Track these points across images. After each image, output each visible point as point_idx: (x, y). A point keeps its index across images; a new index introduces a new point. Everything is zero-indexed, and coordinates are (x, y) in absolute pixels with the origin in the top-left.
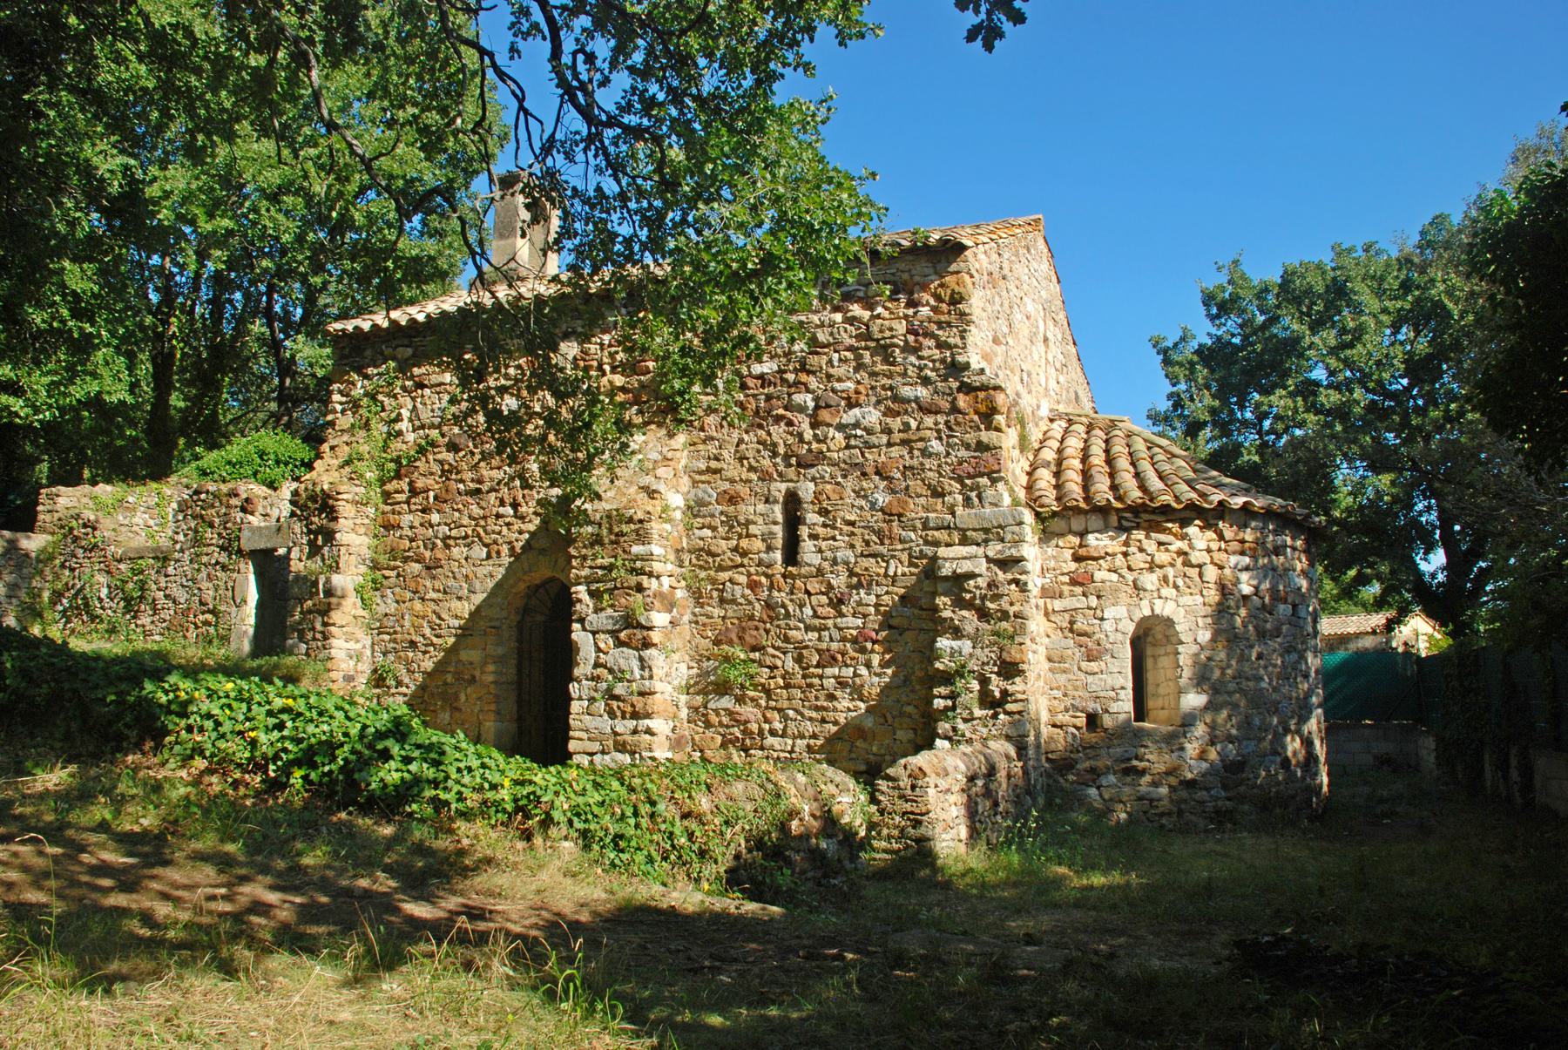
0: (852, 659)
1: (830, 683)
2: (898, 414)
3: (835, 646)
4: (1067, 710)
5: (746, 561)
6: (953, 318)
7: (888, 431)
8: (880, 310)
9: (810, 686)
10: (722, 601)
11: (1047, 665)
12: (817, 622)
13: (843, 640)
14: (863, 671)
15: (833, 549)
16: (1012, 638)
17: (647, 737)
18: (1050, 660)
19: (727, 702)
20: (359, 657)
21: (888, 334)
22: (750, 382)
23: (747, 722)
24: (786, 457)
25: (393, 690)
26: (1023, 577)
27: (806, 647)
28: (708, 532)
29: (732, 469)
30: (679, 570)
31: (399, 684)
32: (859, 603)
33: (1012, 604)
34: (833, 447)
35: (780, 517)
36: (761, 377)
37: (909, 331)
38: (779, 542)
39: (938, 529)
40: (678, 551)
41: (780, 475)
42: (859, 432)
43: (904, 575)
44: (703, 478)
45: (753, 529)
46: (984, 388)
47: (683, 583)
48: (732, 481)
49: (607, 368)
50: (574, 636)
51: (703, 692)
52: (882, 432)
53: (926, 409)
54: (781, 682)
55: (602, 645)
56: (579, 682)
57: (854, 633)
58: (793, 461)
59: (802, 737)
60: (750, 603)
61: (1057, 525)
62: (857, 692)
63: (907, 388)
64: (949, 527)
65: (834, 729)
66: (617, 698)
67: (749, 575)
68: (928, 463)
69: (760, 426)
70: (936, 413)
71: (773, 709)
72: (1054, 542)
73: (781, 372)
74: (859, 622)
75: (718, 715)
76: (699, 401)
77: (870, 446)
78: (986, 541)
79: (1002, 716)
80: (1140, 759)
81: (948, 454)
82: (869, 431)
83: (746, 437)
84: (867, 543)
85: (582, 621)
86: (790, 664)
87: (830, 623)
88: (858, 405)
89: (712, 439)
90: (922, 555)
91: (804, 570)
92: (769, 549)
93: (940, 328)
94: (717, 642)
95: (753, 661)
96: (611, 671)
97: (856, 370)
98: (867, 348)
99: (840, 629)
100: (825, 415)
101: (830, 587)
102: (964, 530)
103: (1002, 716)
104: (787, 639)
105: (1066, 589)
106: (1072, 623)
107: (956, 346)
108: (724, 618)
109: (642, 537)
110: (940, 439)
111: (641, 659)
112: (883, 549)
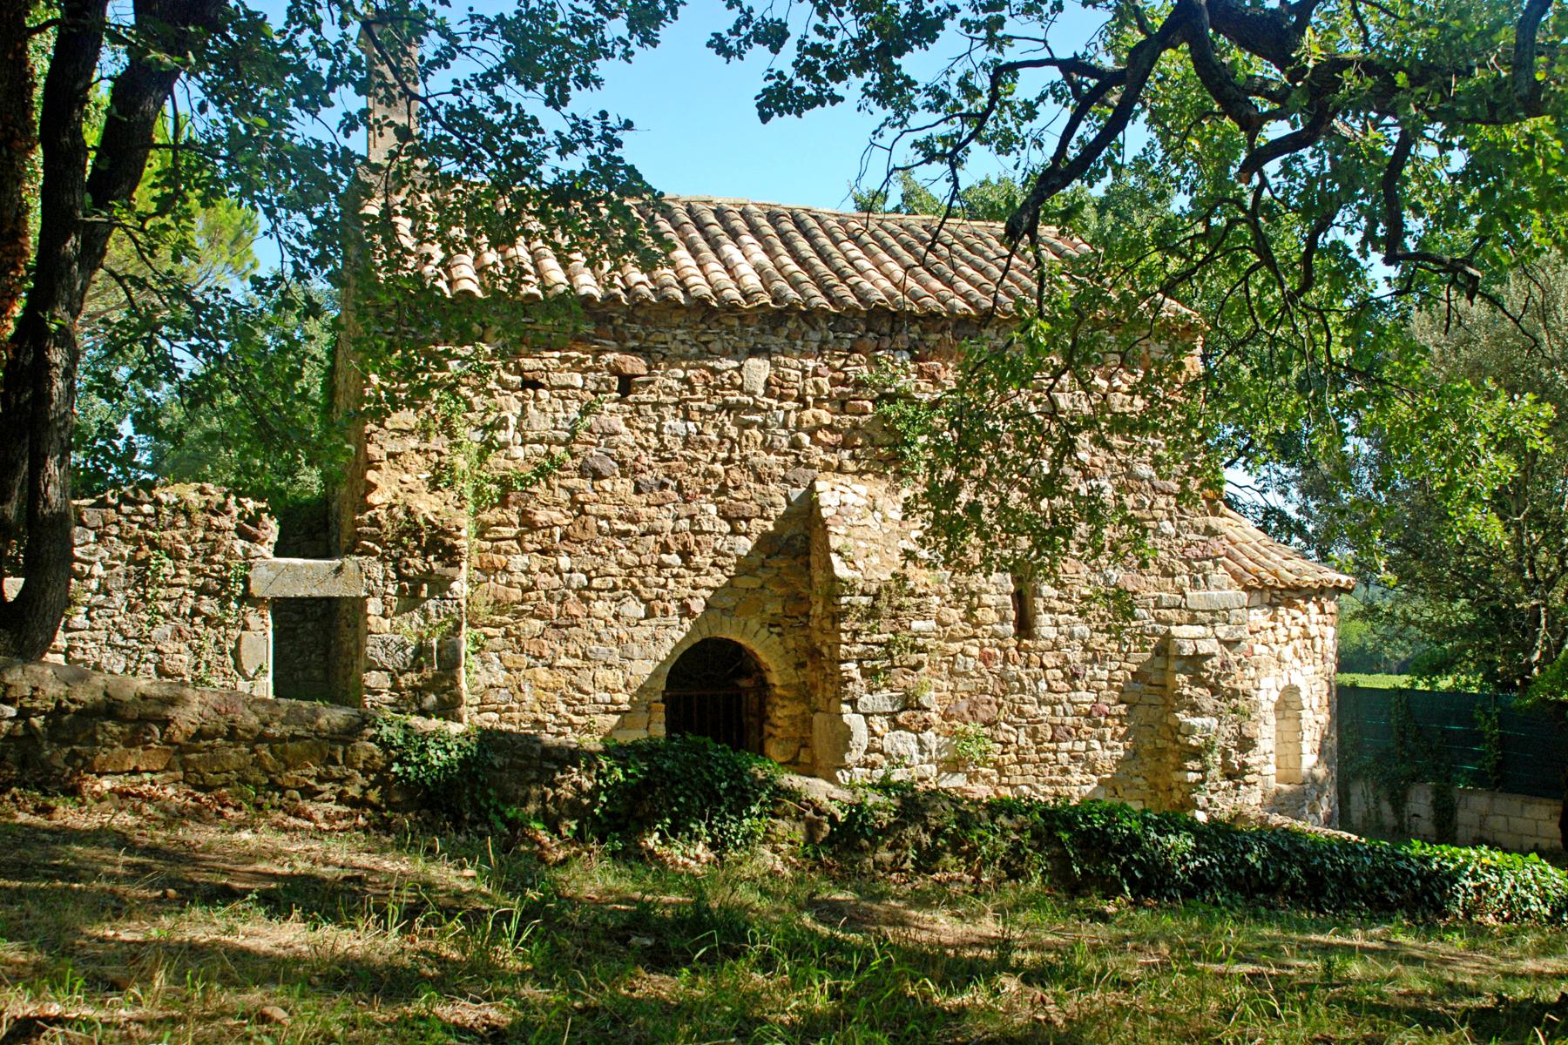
81: (1178, 536)
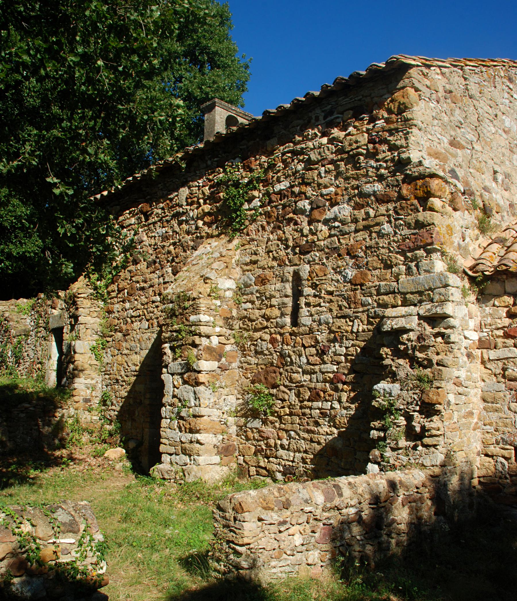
0: (330, 395)
1: (316, 413)
2: (362, 207)
3: (319, 385)
4: (498, 443)
6: (399, 125)
7: (355, 221)
8: (351, 129)
9: (304, 414)
10: (257, 352)
11: (482, 405)
12: (309, 367)
13: (325, 381)
14: (336, 405)
15: (319, 313)
16: (430, 382)
17: (198, 445)
18: (484, 400)
19: (257, 424)
20: (94, 388)
21: (355, 146)
22: (274, 197)
23: (268, 438)
24: (294, 248)
25: (110, 408)
26: (448, 331)
27: (302, 386)
28: (249, 305)
29: (264, 260)
30: (229, 332)
31: (112, 404)
32: (335, 354)
33: (438, 354)
34: (320, 237)
35: (289, 292)
36: (280, 192)
37: (370, 142)
38: (289, 310)
39: (386, 294)
40: (226, 319)
41: (290, 261)
42: (337, 224)
43: (364, 331)
44: (248, 268)
45: (274, 301)
46: (422, 176)
47: (232, 341)
48: (264, 269)
49: (201, 201)
50: (163, 377)
51: (245, 416)
52: (352, 222)
53: (382, 200)
54: (287, 411)
55: (176, 383)
56: (165, 407)
57: (331, 376)
58: (297, 250)
59: (299, 452)
60: (271, 354)
61: (492, 287)
62: (332, 420)
63: (368, 186)
64: (394, 292)
65: (318, 448)
66: (182, 418)
67: (271, 334)
68: (382, 243)
69: (279, 228)
70: (387, 202)
71: (283, 430)
72: (492, 302)
73: (292, 187)
74: (335, 368)
75: (252, 432)
76: (246, 215)
77: (343, 233)
78: (421, 302)
79: (420, 448)
80: (373, 508)
81: (396, 233)
82: (343, 223)
83: (271, 237)
84: (340, 307)
85: (166, 367)
86: (293, 398)
87: (317, 368)
88: (337, 204)
89: (253, 240)
90: (376, 316)
91: (302, 329)
92: (283, 315)
93: (391, 135)
94: (253, 382)
95: (272, 395)
96: (180, 401)
97: (336, 178)
98: (342, 160)
99: (323, 373)
100: (316, 214)
101: (317, 341)
102: (405, 294)
103: (420, 448)
104: (291, 381)
105: (500, 341)
106: (504, 369)
107: (402, 147)
108: (257, 364)
109: (196, 310)
110: (390, 222)
111: (195, 393)
112: (350, 312)
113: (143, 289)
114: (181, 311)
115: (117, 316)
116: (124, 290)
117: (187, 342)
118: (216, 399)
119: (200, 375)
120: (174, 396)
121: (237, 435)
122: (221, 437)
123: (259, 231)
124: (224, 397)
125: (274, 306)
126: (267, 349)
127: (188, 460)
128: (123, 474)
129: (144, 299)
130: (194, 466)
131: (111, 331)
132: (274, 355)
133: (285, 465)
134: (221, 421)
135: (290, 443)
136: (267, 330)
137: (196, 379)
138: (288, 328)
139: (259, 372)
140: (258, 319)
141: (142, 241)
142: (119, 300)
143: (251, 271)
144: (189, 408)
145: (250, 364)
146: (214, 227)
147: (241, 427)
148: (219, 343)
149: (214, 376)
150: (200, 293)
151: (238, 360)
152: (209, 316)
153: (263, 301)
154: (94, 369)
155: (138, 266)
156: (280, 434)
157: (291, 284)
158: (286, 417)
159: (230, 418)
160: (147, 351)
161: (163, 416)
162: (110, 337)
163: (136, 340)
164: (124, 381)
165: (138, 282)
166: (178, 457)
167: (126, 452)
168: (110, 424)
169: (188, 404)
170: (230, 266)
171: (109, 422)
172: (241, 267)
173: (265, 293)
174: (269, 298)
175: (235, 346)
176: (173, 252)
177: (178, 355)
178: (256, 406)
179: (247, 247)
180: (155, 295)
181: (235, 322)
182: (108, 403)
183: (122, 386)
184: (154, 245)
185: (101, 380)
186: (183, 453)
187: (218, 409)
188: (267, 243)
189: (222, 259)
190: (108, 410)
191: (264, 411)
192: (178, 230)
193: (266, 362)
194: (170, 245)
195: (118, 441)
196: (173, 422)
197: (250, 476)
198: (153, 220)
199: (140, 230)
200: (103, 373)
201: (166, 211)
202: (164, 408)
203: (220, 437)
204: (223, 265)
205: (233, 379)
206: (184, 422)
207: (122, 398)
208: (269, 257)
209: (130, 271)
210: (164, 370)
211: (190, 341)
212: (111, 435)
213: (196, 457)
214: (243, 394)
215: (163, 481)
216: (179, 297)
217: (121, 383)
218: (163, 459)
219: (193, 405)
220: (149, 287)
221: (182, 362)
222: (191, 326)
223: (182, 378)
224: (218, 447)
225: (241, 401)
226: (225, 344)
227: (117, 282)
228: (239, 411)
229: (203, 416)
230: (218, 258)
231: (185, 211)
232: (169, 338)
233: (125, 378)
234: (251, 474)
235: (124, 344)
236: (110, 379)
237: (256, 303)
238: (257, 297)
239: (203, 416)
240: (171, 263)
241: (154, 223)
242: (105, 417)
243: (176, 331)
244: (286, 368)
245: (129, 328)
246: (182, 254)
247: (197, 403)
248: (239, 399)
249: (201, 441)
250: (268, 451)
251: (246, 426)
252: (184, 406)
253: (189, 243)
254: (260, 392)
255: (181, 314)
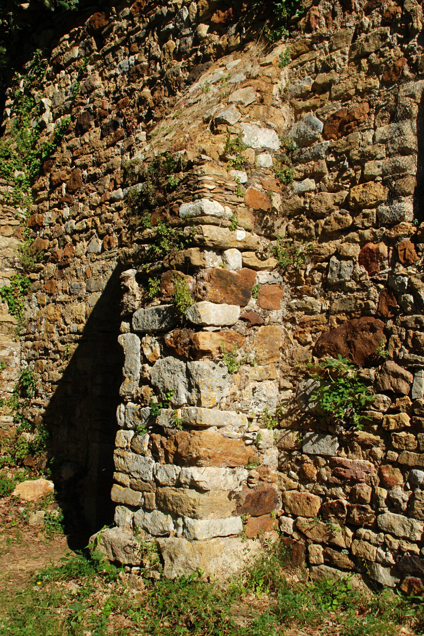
5: (358, 221)
17: (193, 494)
23: (354, 481)
30: (265, 242)
31: (37, 395)
44: (307, 103)
47: (272, 262)
50: (121, 339)
54: (406, 419)
55: (148, 352)
56: (125, 403)
60: (364, 288)
67: (363, 242)
71: (395, 464)
75: (316, 464)
83: (366, 21)
85: (129, 318)
89: (321, 38)
94: (151, 343)
95: (366, 382)
96: (156, 391)
108: (328, 313)
111: (188, 374)
113: (93, 178)
114: (161, 195)
115: (49, 232)
116: (60, 184)
117: (173, 263)
118: (235, 389)
119: (201, 334)
120: (144, 381)
121: (280, 469)
122: (246, 473)
123: (334, 14)
124: (252, 385)
125: (373, 178)
126: (354, 277)
127: (171, 527)
128: (42, 536)
129: (95, 198)
130: (185, 542)
131: (38, 262)
132: (372, 289)
133: (400, 551)
134: (246, 438)
135: (412, 498)
136: (353, 235)
137: (191, 342)
138: (409, 225)
139: (332, 329)
140: (330, 211)
141: (93, 88)
142: (53, 203)
143: (314, 108)
144: (176, 407)
145: (313, 313)
146: (232, 30)
147: (290, 451)
148: (244, 265)
149: (231, 338)
150: (204, 152)
151: (283, 304)
152: (223, 203)
153: (343, 169)
154: (5, 329)
155: (86, 137)
156: (386, 475)
157: (415, 124)
158: (403, 434)
159: (265, 431)
160: (99, 294)
161: (121, 422)
162: (37, 272)
163: (80, 274)
164: (57, 352)
165: (84, 167)
166: (148, 516)
167: (55, 488)
168: (32, 431)
169: (172, 399)
170: (268, 100)
171: (30, 427)
172: (292, 105)
173: (347, 152)
174: (358, 162)
175: (277, 275)
176: (150, 98)
177: (153, 291)
178: (328, 407)
179: (306, 57)
180: (115, 188)
181: (278, 223)
182: (30, 391)
183: (54, 360)
184: (114, 93)
185: (19, 349)
186: (160, 509)
187: (239, 410)
188: (355, 38)
189: (252, 82)
190: (29, 404)
191: (345, 418)
192: (158, 53)
193: (350, 306)
194: (143, 87)
195: (44, 465)
196: (140, 437)
197: (309, 565)
198: (113, 44)
199: (90, 68)
200: (23, 338)
201: (136, 19)
202: (122, 406)
203: (244, 474)
204: (253, 97)
205: (272, 344)
206: (164, 439)
207: (53, 383)
208: (360, 69)
209: (71, 149)
210: (125, 325)
211: (180, 260)
212: (32, 451)
213: (188, 519)
214: (296, 378)
215: (114, 569)
216: (156, 166)
217: (53, 356)
218: (117, 517)
219: (185, 401)
220: (105, 174)
221: (162, 307)
222: (182, 226)
223: (162, 341)
224: (238, 497)
225: (289, 394)
226: (256, 269)
227: (49, 171)
228: (285, 416)
229: (205, 427)
230: (242, 82)
231: (172, 10)
232: (134, 256)
233: (60, 345)
234: (313, 559)
235: (60, 284)
236: (34, 347)
237: (327, 177)
238: (329, 164)
239: (205, 427)
240: (146, 121)
241: (114, 50)
242: (23, 417)
243: (149, 241)
244: (401, 319)
245: (68, 253)
246: (166, 100)
247: (194, 397)
248: (285, 389)
249: (201, 484)
250: (355, 512)
251: (301, 451)
252: (165, 404)
253: (181, 74)
254: (336, 375)
255: (161, 202)
